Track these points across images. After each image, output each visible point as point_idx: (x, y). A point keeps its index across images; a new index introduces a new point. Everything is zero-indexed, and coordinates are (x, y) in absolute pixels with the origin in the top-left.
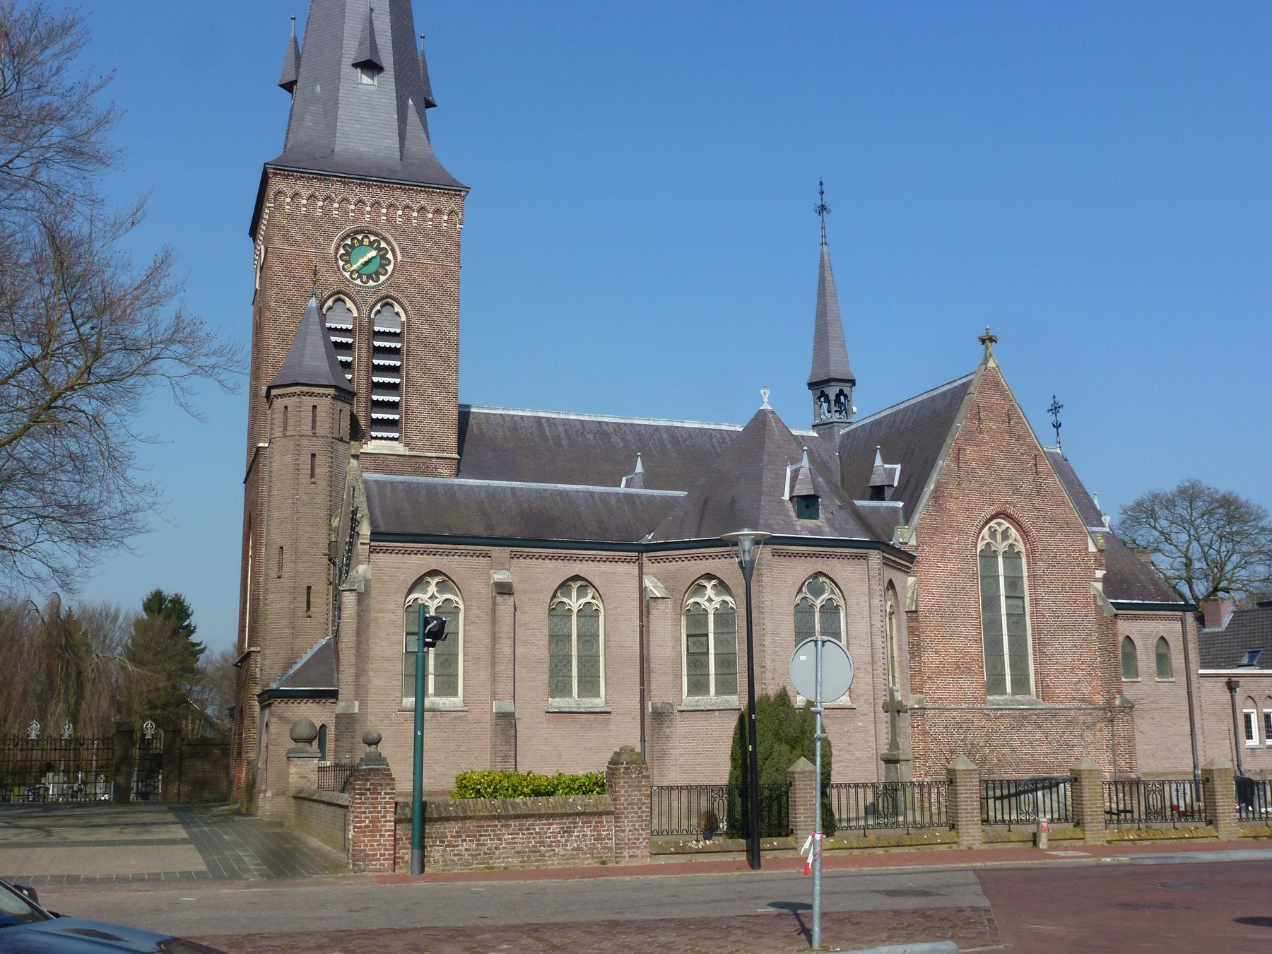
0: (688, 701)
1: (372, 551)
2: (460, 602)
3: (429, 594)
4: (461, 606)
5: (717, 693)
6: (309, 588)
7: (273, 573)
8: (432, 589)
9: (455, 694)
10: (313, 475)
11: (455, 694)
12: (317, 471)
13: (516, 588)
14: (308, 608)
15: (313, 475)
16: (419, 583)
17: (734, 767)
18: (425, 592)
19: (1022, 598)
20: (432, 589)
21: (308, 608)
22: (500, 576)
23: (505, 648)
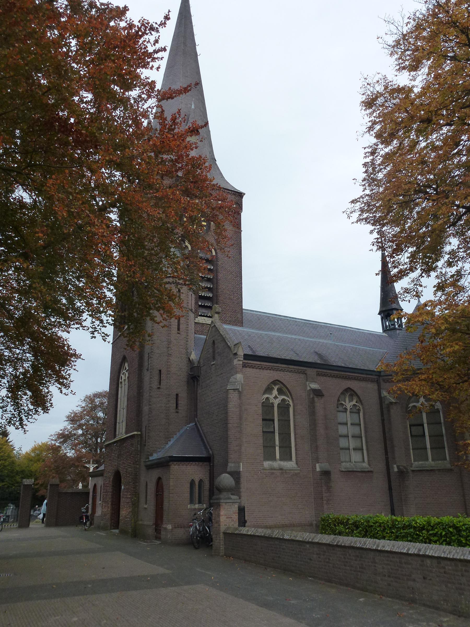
0: (416, 464)
1: (244, 366)
2: (291, 401)
3: (274, 395)
4: (291, 403)
5: (433, 460)
6: (177, 395)
7: (155, 384)
8: (275, 392)
9: (291, 459)
10: (179, 329)
11: (291, 459)
12: (181, 326)
13: (324, 392)
14: (177, 407)
15: (179, 329)
16: (269, 390)
17: (194, 463)
18: (271, 394)
19: (273, 420)
20: (275, 392)
21: (177, 407)
22: (314, 386)
23: (321, 430)
